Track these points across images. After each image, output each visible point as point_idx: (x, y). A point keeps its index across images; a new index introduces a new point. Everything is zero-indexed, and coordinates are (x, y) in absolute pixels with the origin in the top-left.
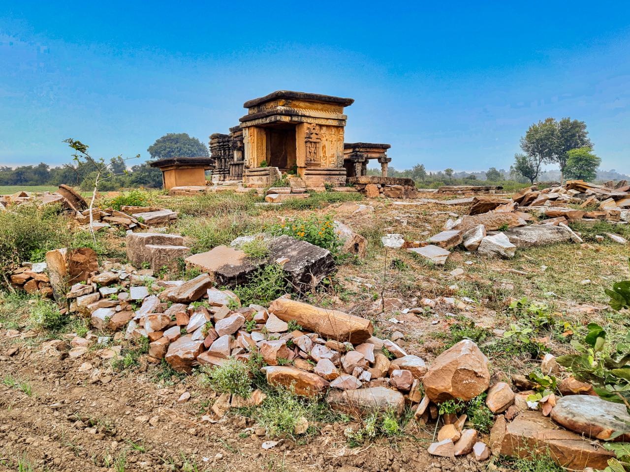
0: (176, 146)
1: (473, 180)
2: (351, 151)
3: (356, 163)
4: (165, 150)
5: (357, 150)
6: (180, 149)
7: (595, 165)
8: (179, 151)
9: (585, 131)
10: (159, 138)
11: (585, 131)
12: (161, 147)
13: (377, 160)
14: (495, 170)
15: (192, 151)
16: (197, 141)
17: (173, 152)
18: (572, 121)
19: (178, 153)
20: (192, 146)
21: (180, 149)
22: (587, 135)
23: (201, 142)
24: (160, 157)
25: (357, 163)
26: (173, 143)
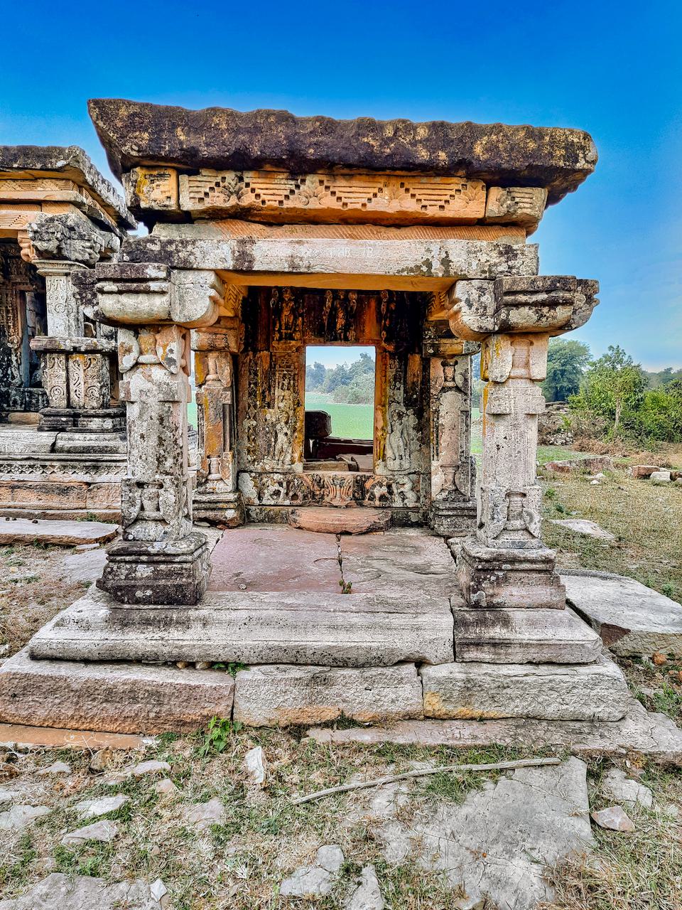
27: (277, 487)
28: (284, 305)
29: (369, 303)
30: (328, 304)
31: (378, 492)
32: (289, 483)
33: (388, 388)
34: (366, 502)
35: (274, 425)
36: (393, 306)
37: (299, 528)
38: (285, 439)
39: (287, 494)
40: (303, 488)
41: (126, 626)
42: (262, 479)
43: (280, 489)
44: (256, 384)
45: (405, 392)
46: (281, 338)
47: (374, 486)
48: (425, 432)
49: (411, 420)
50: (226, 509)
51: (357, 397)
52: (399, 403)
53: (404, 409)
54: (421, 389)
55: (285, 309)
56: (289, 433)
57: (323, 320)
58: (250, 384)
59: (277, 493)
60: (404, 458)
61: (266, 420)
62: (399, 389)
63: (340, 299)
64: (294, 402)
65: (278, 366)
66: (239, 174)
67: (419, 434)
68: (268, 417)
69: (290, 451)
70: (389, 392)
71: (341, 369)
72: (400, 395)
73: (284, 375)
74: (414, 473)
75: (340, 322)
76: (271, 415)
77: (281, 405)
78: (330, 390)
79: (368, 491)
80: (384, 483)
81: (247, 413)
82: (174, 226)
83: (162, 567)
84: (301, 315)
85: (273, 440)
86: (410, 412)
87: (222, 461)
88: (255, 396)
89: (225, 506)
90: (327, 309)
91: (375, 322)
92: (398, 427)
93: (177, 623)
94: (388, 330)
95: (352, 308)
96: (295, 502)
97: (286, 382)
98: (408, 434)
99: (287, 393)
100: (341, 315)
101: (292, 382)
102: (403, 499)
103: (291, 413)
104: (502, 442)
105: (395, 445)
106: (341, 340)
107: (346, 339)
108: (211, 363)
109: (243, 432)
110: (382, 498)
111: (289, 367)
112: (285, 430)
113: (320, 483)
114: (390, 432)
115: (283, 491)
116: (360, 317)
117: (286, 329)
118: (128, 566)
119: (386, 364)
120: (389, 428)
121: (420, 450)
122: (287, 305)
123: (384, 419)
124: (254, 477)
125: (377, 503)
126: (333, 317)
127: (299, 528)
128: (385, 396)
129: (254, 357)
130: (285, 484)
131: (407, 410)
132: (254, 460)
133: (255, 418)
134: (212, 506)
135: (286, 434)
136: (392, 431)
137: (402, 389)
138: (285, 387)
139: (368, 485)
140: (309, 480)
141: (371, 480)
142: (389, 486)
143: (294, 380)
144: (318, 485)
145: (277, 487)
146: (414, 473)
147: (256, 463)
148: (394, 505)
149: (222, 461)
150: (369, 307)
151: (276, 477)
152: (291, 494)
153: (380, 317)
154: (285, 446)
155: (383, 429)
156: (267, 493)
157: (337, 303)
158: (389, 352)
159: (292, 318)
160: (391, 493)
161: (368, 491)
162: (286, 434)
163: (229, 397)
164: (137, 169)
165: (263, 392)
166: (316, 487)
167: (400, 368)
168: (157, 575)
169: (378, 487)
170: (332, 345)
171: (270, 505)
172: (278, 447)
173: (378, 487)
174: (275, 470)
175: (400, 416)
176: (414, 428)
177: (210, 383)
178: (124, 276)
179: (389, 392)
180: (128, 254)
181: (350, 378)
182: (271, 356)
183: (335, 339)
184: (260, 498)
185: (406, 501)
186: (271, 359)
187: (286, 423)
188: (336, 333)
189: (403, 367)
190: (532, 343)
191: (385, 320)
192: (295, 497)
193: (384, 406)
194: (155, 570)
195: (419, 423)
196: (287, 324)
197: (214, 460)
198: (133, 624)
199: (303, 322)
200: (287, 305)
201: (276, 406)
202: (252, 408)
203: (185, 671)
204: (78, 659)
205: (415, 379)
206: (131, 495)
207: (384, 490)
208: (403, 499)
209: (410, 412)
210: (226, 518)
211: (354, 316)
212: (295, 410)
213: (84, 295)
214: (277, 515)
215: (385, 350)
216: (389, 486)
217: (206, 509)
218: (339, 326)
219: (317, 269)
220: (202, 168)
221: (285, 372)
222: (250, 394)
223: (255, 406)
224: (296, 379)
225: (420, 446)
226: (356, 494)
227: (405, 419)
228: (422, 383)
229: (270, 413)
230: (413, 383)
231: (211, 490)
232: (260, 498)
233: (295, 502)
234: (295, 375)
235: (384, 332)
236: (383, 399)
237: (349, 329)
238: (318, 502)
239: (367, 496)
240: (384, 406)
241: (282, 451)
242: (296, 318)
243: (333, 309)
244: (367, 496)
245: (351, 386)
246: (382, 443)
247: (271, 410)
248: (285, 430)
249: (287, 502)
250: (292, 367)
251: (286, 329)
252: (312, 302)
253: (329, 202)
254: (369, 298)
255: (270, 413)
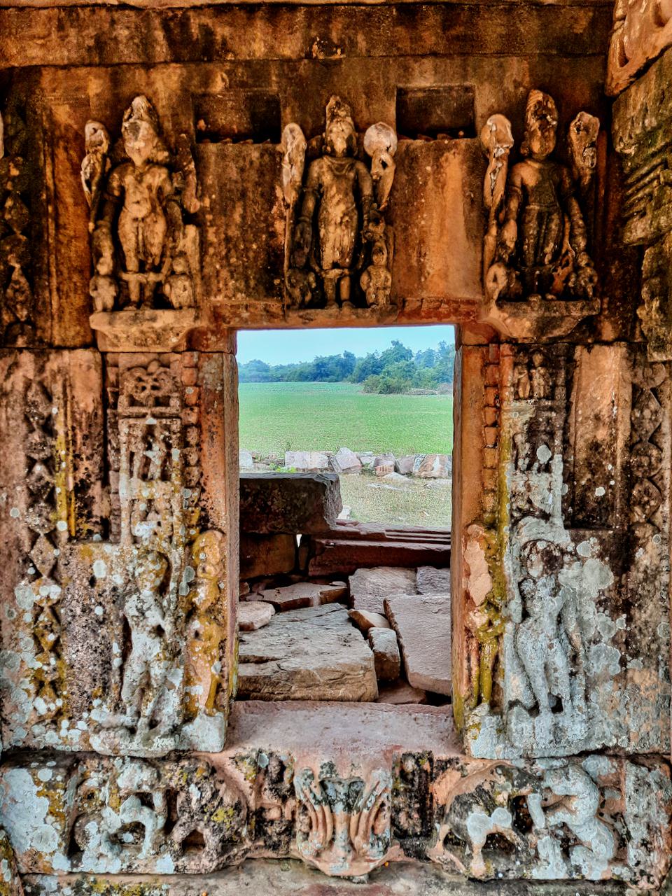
27: (129, 813)
28: (129, 180)
29: (438, 167)
30: (291, 173)
31: (477, 825)
32: (171, 796)
33: (508, 466)
36: (528, 174)
38: (156, 647)
39: (168, 828)
40: (220, 816)
42: (84, 778)
43: (145, 817)
44: (50, 463)
45: (569, 477)
46: (120, 303)
47: (464, 804)
49: (590, 575)
51: (388, 387)
52: (546, 516)
53: (563, 538)
54: (627, 468)
55: (131, 198)
56: (168, 627)
57: (273, 235)
58: (31, 463)
60: (566, 705)
61: (93, 582)
62: (547, 469)
63: (333, 154)
64: (185, 516)
65: (123, 400)
67: (620, 623)
68: (100, 570)
69: (177, 681)
70: (512, 480)
71: (373, 357)
72: (549, 490)
74: (602, 752)
75: (337, 239)
76: (107, 563)
78: (360, 379)
80: (502, 798)
81: (27, 560)
84: (190, 218)
85: (116, 649)
86: (589, 546)
88: (51, 501)
90: (287, 193)
91: (461, 233)
92: (545, 606)
94: (514, 262)
95: (376, 185)
97: (156, 454)
98: (581, 623)
99: (158, 490)
101: (176, 453)
102: (566, 853)
103: (176, 555)
105: (535, 665)
106: (339, 302)
107: (359, 300)
109: (17, 622)
110: (496, 844)
112: (154, 618)
113: (276, 777)
114: (517, 617)
115: (152, 822)
116: (408, 222)
117: (142, 269)
119: (497, 386)
120: (515, 606)
121: (622, 678)
122: (139, 180)
123: (494, 570)
124: (51, 786)
125: (478, 867)
126: (308, 217)
128: (498, 492)
129: (41, 370)
130: (158, 800)
131: (577, 540)
132: (59, 713)
133: (54, 574)
135: (159, 631)
136: (526, 615)
137: (558, 467)
138: (155, 470)
139: (443, 790)
140: (242, 775)
141: (452, 776)
142: (517, 804)
143: (184, 443)
144: (276, 792)
145: (129, 813)
146: (602, 752)
147: (65, 723)
148: (536, 873)
150: (441, 185)
152: (179, 834)
153: (482, 217)
154: (157, 671)
155: (489, 604)
156: (95, 841)
157: (322, 170)
158: (512, 341)
159: (160, 227)
160: (523, 824)
162: (159, 631)
165: (81, 488)
166: (268, 798)
167: (550, 396)
169: (477, 812)
170: (307, 323)
172: (134, 672)
173: (477, 812)
175: (552, 562)
176: (600, 603)
179: (512, 480)
181: (381, 367)
182: (104, 366)
183: (320, 302)
184: (73, 851)
185: (577, 856)
186: (104, 376)
187: (162, 590)
188: (320, 281)
189: (560, 392)
191: (501, 225)
192: (192, 843)
193: (493, 526)
195: (619, 586)
196: (143, 249)
199: (203, 245)
200: (139, 180)
201: (125, 531)
202: (43, 543)
205: (602, 434)
207: (502, 821)
208: (566, 853)
209: (589, 546)
211: (387, 216)
212: (190, 544)
215: (495, 337)
216: (517, 804)
218: (330, 254)
221: (150, 421)
222: (34, 497)
223: (52, 537)
224: (193, 436)
225: (623, 662)
226: (402, 817)
227: (568, 573)
228: (630, 447)
229: (106, 558)
230: (595, 446)
232: (73, 851)
234: (185, 428)
235: (499, 271)
236: (490, 502)
237: (369, 262)
238: (275, 847)
240: (493, 526)
241: (145, 686)
242: (172, 229)
243: (309, 189)
244: (442, 830)
245: (382, 375)
246: (487, 649)
247: (107, 548)
248: (154, 618)
250: (175, 402)
251: (142, 269)
252: (233, 173)
254: (440, 151)
255: (106, 558)
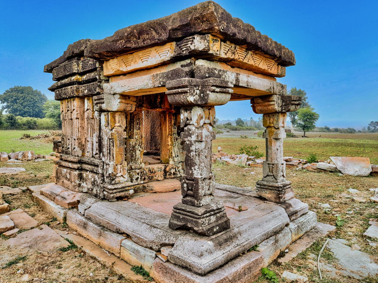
0: (21, 95)
1: (230, 126)
2: (167, 52)
3: (189, 107)
4: (12, 97)
5: (198, 43)
6: (25, 98)
7: (315, 119)
8: (23, 99)
9: (306, 96)
10: (8, 89)
11: (306, 96)
12: (9, 96)
13: (249, 101)
14: (241, 120)
15: (33, 99)
16: (40, 92)
17: (19, 100)
18: (298, 89)
19: (23, 101)
20: (35, 96)
21: (25, 98)
22: (306, 100)
23: (42, 93)
24: (8, 103)
25: (115, 109)
26: (20, 93)
34: (168, 176)
35: (134, 147)
37: (155, 192)
41: (221, 245)
47: (170, 169)
48: (184, 145)
50: (129, 190)
59: (137, 179)
61: (130, 144)
66: (235, 46)
70: (173, 130)
73: (137, 123)
77: (136, 137)
79: (168, 172)
82: (209, 62)
83: (218, 215)
85: (134, 153)
87: (123, 166)
89: (129, 188)
93: (234, 237)
96: (145, 181)
100: (159, 97)
104: (278, 148)
108: (117, 118)
110: (174, 174)
111: (139, 119)
118: (208, 218)
125: (173, 176)
127: (155, 192)
134: (123, 189)
145: (137, 176)
149: (123, 166)
151: (138, 171)
152: (143, 178)
161: (168, 172)
162: (140, 150)
163: (126, 134)
164: (209, 35)
168: (218, 219)
171: (136, 185)
174: (136, 168)
177: (116, 127)
178: (222, 85)
180: (208, 73)
190: (274, 116)
192: (144, 179)
194: (217, 217)
197: (119, 166)
198: (223, 243)
201: (134, 138)
203: (248, 253)
204: (195, 269)
206: (202, 185)
210: (130, 194)
213: (191, 91)
214: (138, 189)
217: (119, 192)
219: (252, 87)
220: (228, 40)
221: (138, 122)
231: (118, 182)
233: (145, 181)
239: (168, 174)
249: (142, 182)
253: (251, 62)
